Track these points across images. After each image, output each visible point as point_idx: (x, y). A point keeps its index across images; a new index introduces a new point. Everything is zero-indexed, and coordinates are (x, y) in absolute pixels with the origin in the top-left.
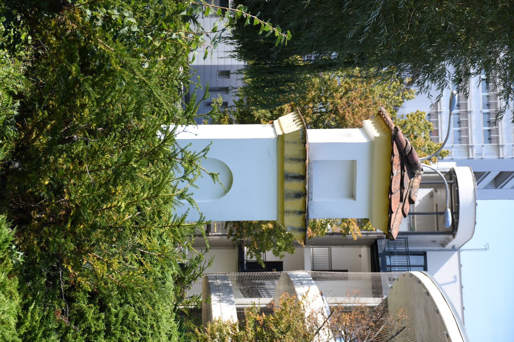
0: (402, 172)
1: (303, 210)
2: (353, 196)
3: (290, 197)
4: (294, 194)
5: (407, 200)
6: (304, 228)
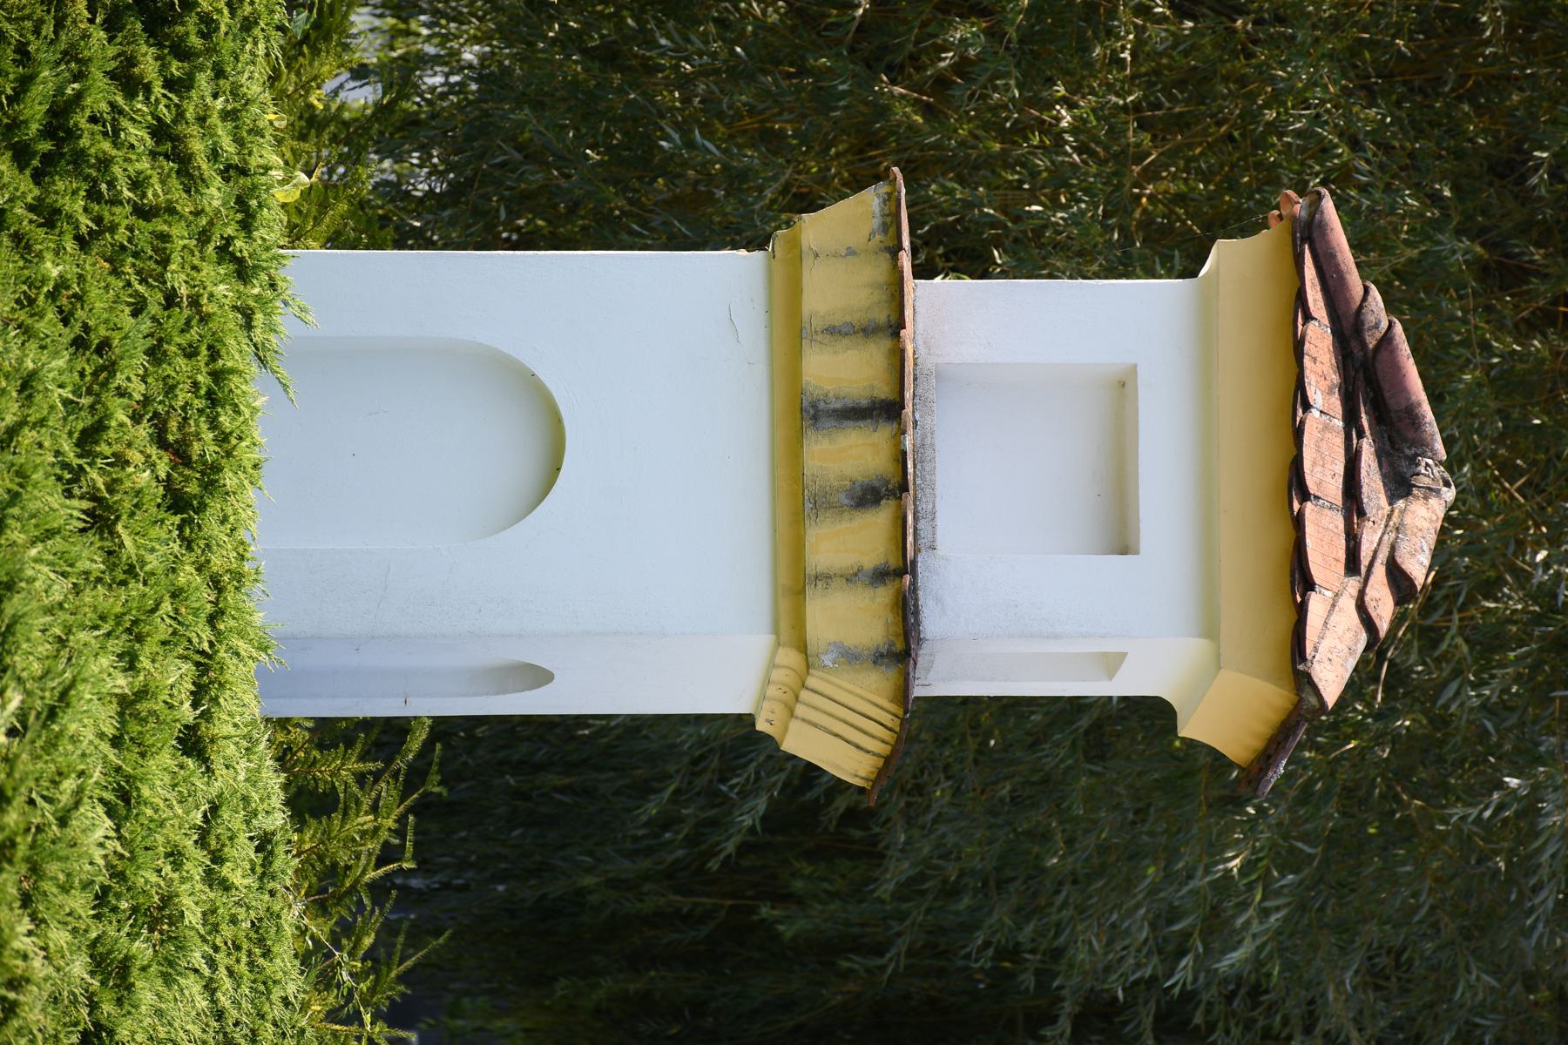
0: (1348, 438)
1: (894, 562)
2: (1122, 543)
3: (831, 506)
4: (850, 492)
5: (1380, 572)
6: (899, 646)
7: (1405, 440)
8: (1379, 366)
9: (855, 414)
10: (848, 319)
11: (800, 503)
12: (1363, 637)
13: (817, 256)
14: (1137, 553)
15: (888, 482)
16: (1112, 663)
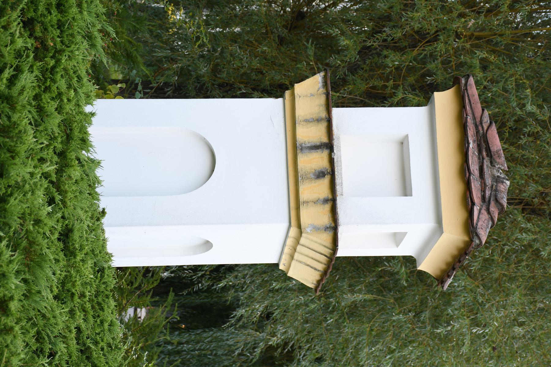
3: (308, 178)
7: (496, 162)
8: (488, 136)
10: (312, 116)
12: (491, 223)
13: (300, 97)
14: (411, 195)
15: (327, 170)
16: (397, 238)
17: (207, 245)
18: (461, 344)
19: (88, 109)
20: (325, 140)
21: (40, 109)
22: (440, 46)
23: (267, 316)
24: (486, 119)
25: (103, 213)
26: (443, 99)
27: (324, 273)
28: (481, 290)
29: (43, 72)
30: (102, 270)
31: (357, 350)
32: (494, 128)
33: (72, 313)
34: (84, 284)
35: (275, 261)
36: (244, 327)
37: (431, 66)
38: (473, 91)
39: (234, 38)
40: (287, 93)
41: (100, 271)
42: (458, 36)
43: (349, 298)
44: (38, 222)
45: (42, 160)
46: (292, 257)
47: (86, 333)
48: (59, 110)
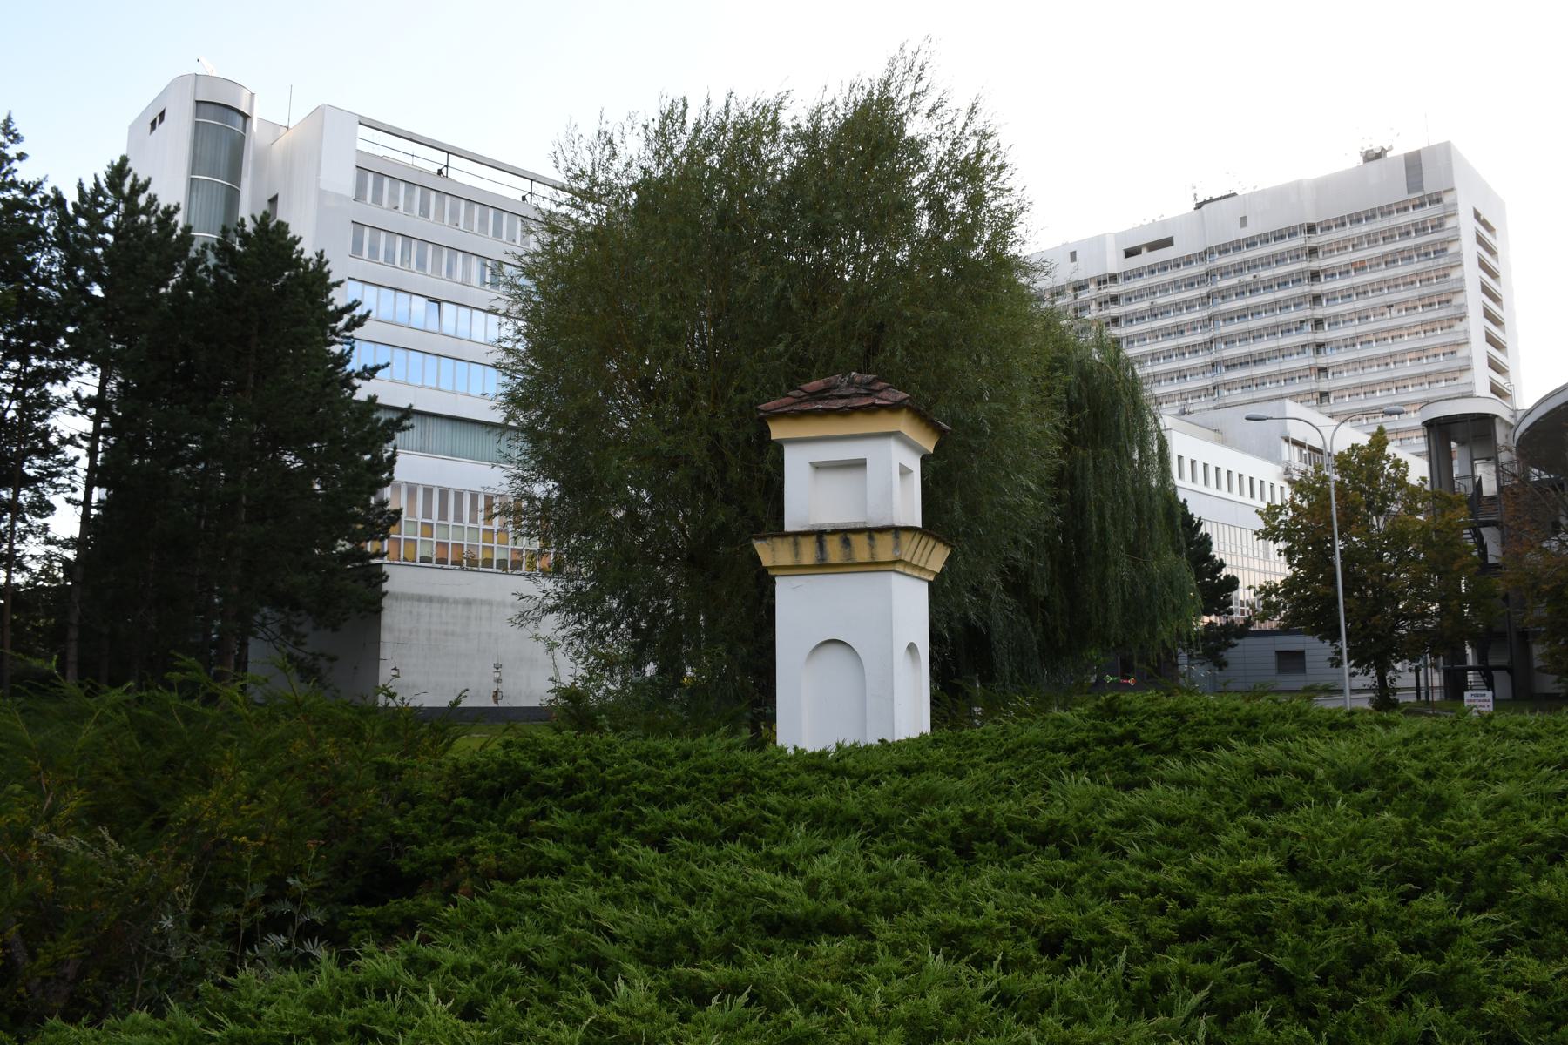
2: (860, 464)
9: (821, 547)
11: (850, 566)
16: (905, 472)
17: (912, 648)
18: (1001, 413)
19: (790, 751)
20: (814, 538)
21: (796, 790)
22: (723, 431)
23: (975, 590)
24: (796, 393)
25: (882, 741)
26: (777, 432)
27: (938, 539)
28: (949, 392)
29: (764, 787)
30: (936, 742)
31: (1006, 506)
32: (805, 386)
33: (974, 766)
34: (948, 756)
35: (925, 586)
36: (987, 612)
37: (741, 438)
38: (770, 405)
39: (711, 620)
40: (771, 573)
41: (936, 743)
42: (714, 415)
43: (958, 512)
44: (896, 793)
45: (841, 789)
46: (923, 569)
47: (991, 753)
48: (796, 775)
